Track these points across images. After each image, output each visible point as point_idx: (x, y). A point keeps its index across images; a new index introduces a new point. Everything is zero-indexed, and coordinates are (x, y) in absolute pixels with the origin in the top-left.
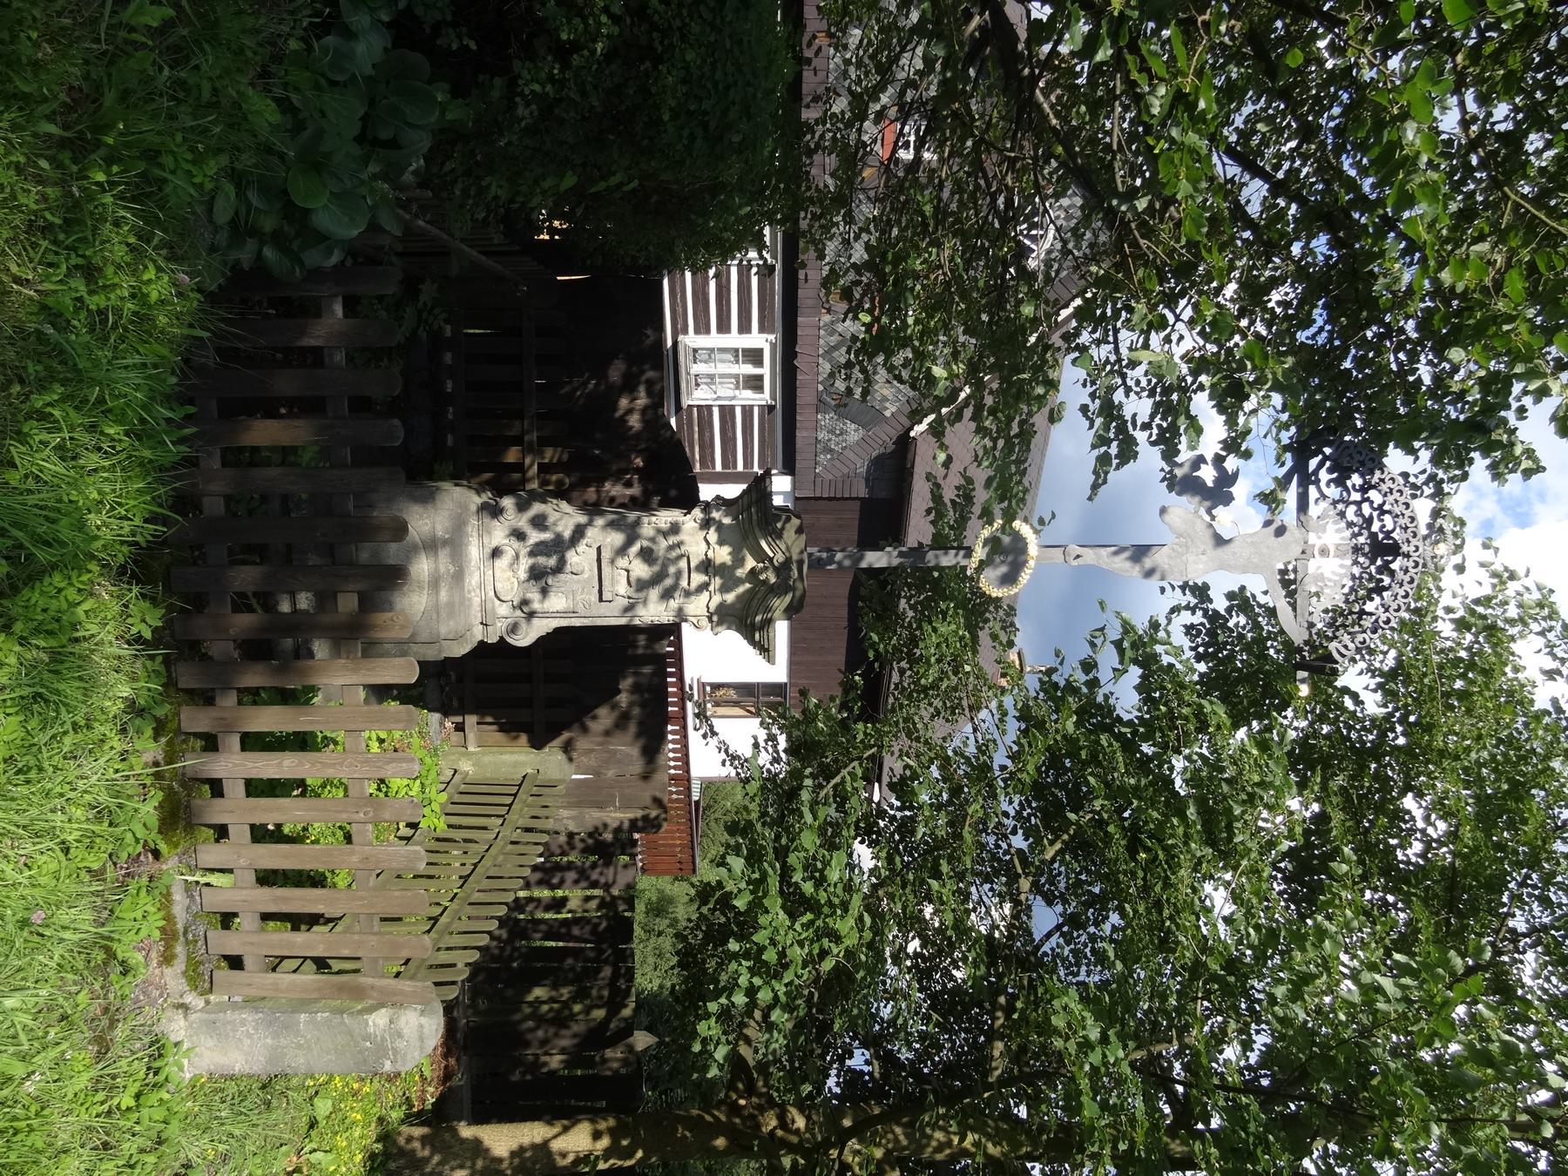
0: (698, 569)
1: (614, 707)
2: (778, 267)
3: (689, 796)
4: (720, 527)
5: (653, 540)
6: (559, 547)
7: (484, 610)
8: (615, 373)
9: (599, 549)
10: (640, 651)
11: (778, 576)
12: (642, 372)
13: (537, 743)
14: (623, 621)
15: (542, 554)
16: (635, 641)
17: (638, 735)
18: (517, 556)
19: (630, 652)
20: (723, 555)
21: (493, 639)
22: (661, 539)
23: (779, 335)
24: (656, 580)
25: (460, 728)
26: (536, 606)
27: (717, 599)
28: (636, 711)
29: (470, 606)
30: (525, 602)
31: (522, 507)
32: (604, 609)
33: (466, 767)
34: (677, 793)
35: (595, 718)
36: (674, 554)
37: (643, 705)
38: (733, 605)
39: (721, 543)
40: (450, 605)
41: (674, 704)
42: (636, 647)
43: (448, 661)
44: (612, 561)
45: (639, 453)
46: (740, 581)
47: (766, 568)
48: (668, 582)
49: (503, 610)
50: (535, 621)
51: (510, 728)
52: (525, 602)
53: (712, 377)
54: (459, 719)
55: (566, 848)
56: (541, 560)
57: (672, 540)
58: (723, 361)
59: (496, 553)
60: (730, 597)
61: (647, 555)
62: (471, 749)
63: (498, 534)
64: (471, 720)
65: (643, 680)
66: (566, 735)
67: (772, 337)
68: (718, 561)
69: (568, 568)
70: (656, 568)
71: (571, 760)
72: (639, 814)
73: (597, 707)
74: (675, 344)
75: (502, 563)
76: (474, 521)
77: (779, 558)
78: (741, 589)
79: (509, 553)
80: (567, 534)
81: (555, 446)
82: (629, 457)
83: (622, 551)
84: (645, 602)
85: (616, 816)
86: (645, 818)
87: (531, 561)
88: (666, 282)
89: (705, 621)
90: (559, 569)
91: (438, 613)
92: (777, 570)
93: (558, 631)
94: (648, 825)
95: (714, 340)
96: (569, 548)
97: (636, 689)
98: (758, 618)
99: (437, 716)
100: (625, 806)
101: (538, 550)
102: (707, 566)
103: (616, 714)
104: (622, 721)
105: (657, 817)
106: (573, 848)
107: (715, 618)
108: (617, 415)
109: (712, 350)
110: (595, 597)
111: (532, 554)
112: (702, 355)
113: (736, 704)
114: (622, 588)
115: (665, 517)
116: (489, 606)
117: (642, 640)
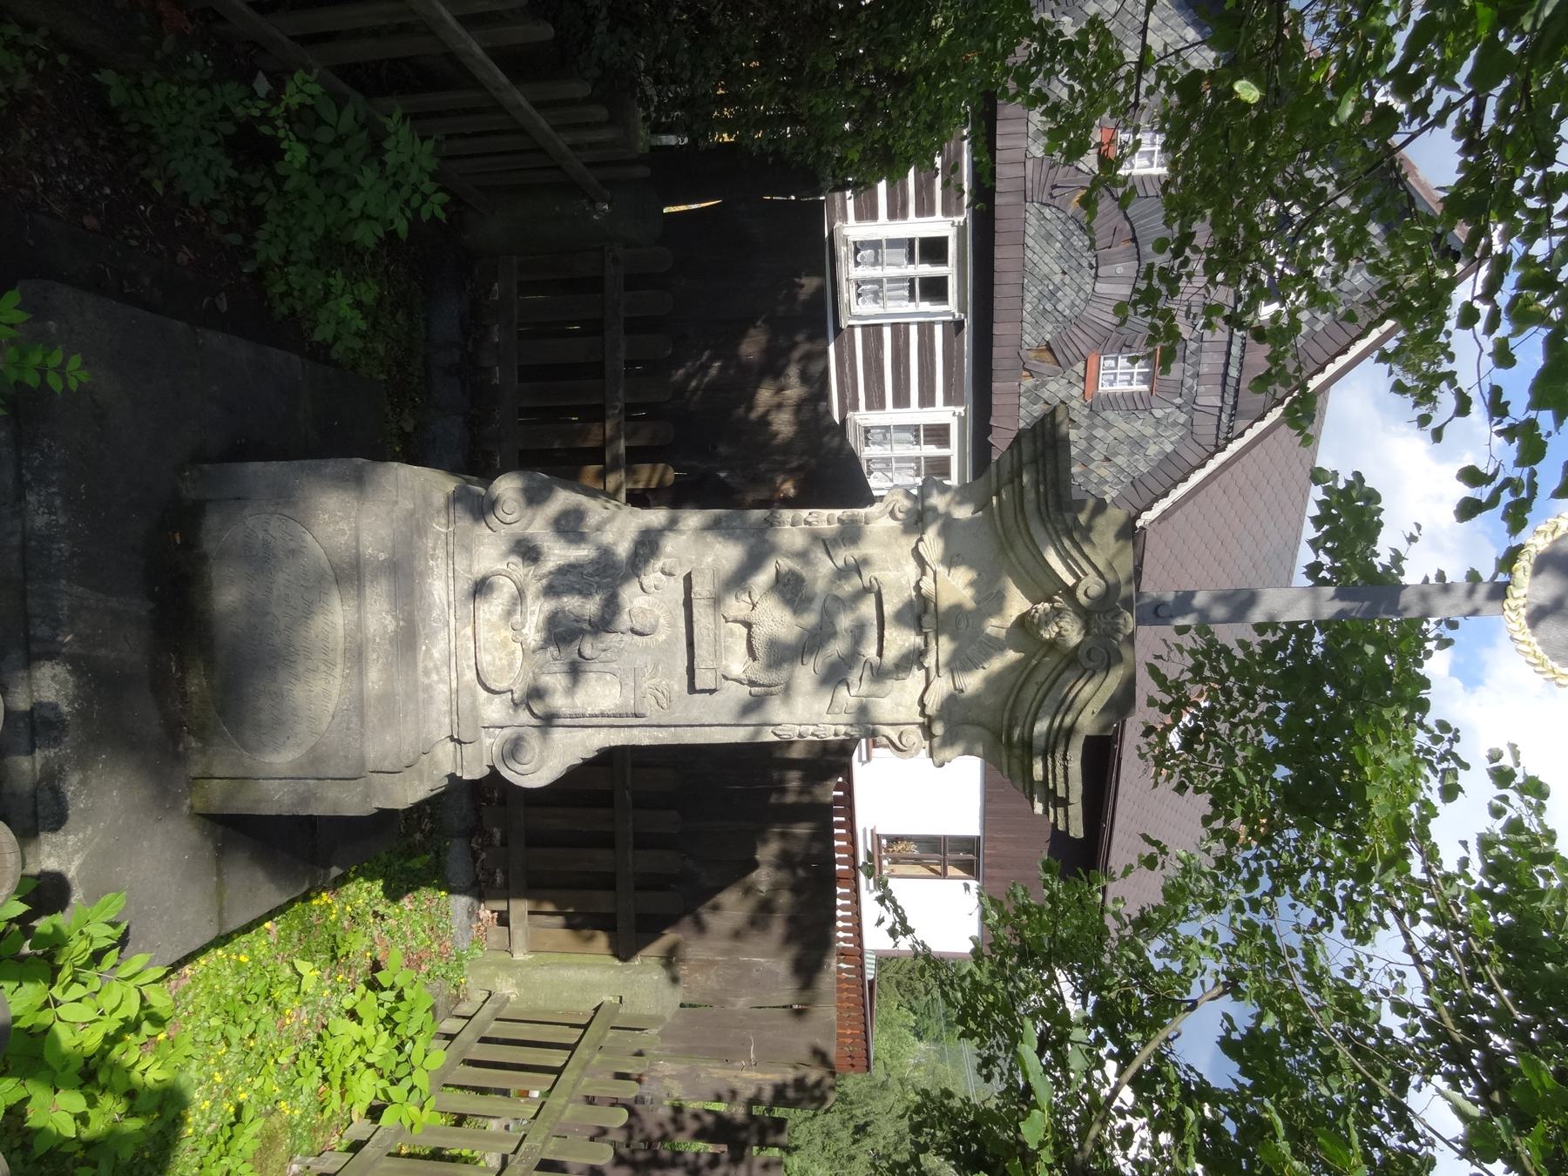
0: (900, 618)
1: (749, 891)
2: (968, 323)
3: (862, 976)
4: (949, 528)
5: (803, 556)
6: (607, 576)
7: (456, 712)
8: (751, 348)
9: (688, 579)
10: (791, 798)
12: (794, 345)
13: (624, 951)
14: (738, 735)
15: (571, 590)
16: (782, 781)
17: (788, 939)
18: (521, 594)
19: (773, 799)
20: (955, 587)
21: (474, 771)
22: (820, 555)
23: (970, 407)
25: (503, 920)
26: (559, 702)
27: (942, 687)
28: (784, 899)
29: (429, 700)
30: (536, 693)
31: (534, 497)
32: (699, 708)
33: (507, 988)
34: (847, 971)
35: (716, 908)
36: (848, 588)
37: (796, 889)
38: (977, 698)
39: (950, 561)
40: (387, 698)
41: (843, 861)
42: (783, 791)
43: (386, 817)
44: (716, 601)
45: (791, 473)
47: (1058, 613)
48: (837, 648)
49: (494, 710)
50: (558, 734)
51: (580, 923)
52: (536, 693)
53: (887, 461)
54: (501, 905)
55: (670, 1128)
56: (571, 603)
57: (845, 555)
58: (900, 442)
59: (481, 588)
60: (972, 682)
61: (790, 590)
62: (519, 956)
63: (488, 552)
64: (519, 908)
65: (796, 848)
66: (670, 937)
67: (960, 410)
68: (945, 601)
69: (624, 621)
70: (810, 619)
71: (675, 980)
72: (790, 1075)
73: (720, 889)
74: (844, 421)
75: (492, 608)
76: (439, 527)
77: (1091, 586)
78: (996, 664)
79: (506, 589)
80: (623, 550)
81: (654, 461)
82: (772, 481)
83: (738, 580)
84: (787, 690)
85: (754, 1078)
86: (799, 1083)
87: (548, 606)
88: (832, 349)
89: (915, 736)
90: (604, 624)
91: (362, 716)
92: (1086, 615)
93: (608, 757)
94: (805, 1094)
95: (890, 415)
96: (626, 578)
97: (785, 861)
98: (1041, 727)
99: (461, 903)
100: (766, 1059)
101: (563, 582)
102: (920, 613)
103: (751, 903)
105: (818, 1084)
106: (680, 1128)
107: (938, 729)
108: (754, 415)
109: (887, 428)
110: (679, 684)
111: (551, 591)
112: (876, 435)
113: (917, 861)
114: (738, 664)
115: (826, 519)
116: (465, 701)
117: (794, 779)
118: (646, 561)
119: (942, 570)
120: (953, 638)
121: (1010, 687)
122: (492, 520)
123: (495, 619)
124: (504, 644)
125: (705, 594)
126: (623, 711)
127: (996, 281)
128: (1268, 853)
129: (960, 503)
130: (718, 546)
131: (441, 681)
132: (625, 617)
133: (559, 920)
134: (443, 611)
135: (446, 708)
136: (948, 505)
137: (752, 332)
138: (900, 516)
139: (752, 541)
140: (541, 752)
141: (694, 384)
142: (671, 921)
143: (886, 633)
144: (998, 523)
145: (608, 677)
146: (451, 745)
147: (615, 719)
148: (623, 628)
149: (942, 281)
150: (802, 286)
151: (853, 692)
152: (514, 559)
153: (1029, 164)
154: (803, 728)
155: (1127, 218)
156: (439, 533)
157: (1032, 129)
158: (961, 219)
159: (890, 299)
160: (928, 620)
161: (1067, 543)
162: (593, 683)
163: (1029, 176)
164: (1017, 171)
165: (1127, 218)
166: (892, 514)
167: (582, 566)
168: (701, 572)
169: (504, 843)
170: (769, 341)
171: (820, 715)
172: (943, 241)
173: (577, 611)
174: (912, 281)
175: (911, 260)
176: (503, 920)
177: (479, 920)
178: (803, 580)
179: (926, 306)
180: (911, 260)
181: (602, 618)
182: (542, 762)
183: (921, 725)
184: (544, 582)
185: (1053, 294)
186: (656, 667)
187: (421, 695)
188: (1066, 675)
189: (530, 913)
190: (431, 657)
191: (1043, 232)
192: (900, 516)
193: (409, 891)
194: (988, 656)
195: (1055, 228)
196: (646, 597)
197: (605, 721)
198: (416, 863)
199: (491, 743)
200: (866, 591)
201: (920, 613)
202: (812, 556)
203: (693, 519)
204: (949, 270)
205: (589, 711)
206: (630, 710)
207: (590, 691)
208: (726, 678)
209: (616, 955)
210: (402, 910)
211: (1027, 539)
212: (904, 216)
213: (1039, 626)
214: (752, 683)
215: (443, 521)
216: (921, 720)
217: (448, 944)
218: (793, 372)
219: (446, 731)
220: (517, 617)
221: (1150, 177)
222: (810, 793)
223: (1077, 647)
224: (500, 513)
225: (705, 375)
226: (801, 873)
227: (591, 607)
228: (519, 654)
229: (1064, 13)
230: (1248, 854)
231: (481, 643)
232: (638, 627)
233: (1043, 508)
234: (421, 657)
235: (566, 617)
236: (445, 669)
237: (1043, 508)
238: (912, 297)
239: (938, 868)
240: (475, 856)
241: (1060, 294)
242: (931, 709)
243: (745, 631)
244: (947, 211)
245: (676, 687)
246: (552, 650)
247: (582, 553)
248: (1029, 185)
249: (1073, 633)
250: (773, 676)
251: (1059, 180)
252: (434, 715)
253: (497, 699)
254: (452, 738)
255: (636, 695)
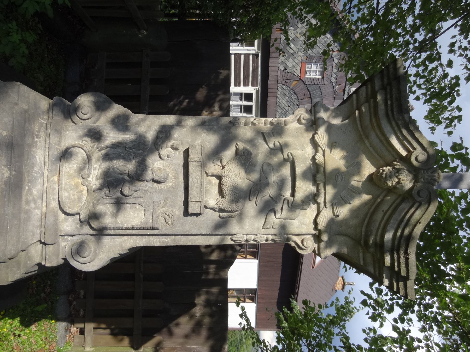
0: (305, 175)
4: (330, 129)
5: (251, 141)
6: (140, 150)
7: (44, 226)
9: (187, 153)
10: (211, 277)
11: (416, 179)
12: (217, 95)
14: (213, 241)
15: (118, 157)
16: (208, 269)
17: (208, 338)
18: (89, 159)
19: (203, 277)
20: (335, 159)
24: (254, 190)
25: (82, 332)
26: (108, 221)
27: (326, 215)
28: (207, 320)
29: (28, 219)
31: (100, 107)
32: (190, 224)
35: (177, 325)
36: (276, 159)
37: (211, 315)
38: (345, 221)
39: (332, 145)
42: (208, 273)
46: (356, 192)
47: (398, 171)
48: (270, 192)
50: (107, 240)
54: (81, 326)
56: (119, 164)
57: (274, 142)
59: (66, 155)
60: (343, 212)
61: (244, 159)
62: (88, 349)
63: (72, 135)
64: (89, 327)
65: (213, 298)
66: (157, 338)
68: (330, 166)
69: (149, 175)
70: (255, 176)
73: (179, 316)
75: (70, 167)
76: (43, 120)
78: (356, 202)
79: (81, 155)
80: (150, 135)
83: (215, 154)
84: (241, 217)
87: (105, 165)
90: (137, 177)
92: (415, 172)
97: (208, 304)
98: (389, 236)
99: (62, 325)
101: (116, 152)
102: (316, 173)
104: (197, 328)
107: (325, 237)
110: (179, 210)
111: (107, 157)
114: (213, 200)
116: (50, 219)
117: (212, 268)
118: (163, 142)
119: (327, 150)
120: (335, 186)
121: (366, 215)
122: (76, 119)
123: (72, 172)
124: (76, 186)
125: (197, 159)
126: (145, 226)
127: (268, 108)
128: (396, 297)
129: (335, 117)
130: (204, 135)
131: (36, 208)
132: (149, 172)
133: (108, 331)
134: (41, 168)
135: (38, 224)
136: (329, 118)
137: (201, 89)
138: (303, 122)
139: (223, 132)
140: (95, 250)
141: (176, 108)
142: (158, 331)
143: (297, 183)
144: (359, 126)
145: (138, 206)
146: (40, 246)
147: (140, 230)
148: (148, 178)
149: (251, 107)
150: (221, 73)
151: (278, 216)
152: (88, 139)
153: (279, 72)
154: (248, 237)
155: (308, 91)
156: (42, 123)
157: (280, 61)
158: (257, 88)
159: (234, 112)
160: (320, 177)
161: (405, 132)
162: (129, 210)
163: (279, 76)
164: (275, 74)
165: (308, 91)
166: (299, 121)
167: (126, 143)
168: (195, 147)
169: (85, 297)
170: (208, 93)
171: (258, 229)
172: (251, 95)
173: (122, 168)
174: (241, 106)
175: (241, 100)
176: (82, 332)
177: (71, 332)
178: (251, 154)
179: (245, 115)
180: (241, 100)
181: (136, 173)
182: (95, 256)
183: (314, 235)
184: (103, 152)
185: (285, 113)
186: (165, 201)
187: (23, 216)
188: (403, 206)
189: (94, 328)
190: (31, 194)
191: (283, 93)
192: (303, 122)
193: (36, 321)
194: (352, 198)
195: (287, 92)
196: (162, 162)
197: (134, 232)
198: (40, 308)
199: (66, 245)
200: (285, 160)
201: (316, 173)
202: (256, 141)
203: (190, 121)
204: (253, 104)
205: (125, 225)
206: (149, 225)
207: (126, 214)
208: (206, 207)
209: (132, 347)
210: (31, 331)
211: (378, 131)
212: (239, 86)
213: (386, 179)
214: (221, 210)
215: (46, 117)
216: (314, 232)
217: (54, 345)
218: (217, 106)
219: (37, 238)
220: (86, 171)
221: (316, 78)
222: (219, 274)
223: (411, 189)
224: (80, 114)
225: (181, 104)
226: (214, 308)
227: (129, 167)
228: (85, 192)
229: (291, 26)
230: (387, 298)
231: (63, 186)
232: (156, 178)
233: (390, 113)
234: (24, 193)
235: (115, 171)
236: (40, 201)
237: (390, 113)
238: (241, 112)
239: (244, 256)
240: (70, 303)
241: (287, 113)
242: (321, 226)
243: (217, 181)
244: (253, 85)
245: (177, 213)
246: (106, 191)
247: (127, 137)
248: (279, 78)
249: (407, 182)
250: (234, 207)
251: (288, 77)
252: (31, 228)
253: (70, 219)
254: (41, 243)
255: (151, 217)
